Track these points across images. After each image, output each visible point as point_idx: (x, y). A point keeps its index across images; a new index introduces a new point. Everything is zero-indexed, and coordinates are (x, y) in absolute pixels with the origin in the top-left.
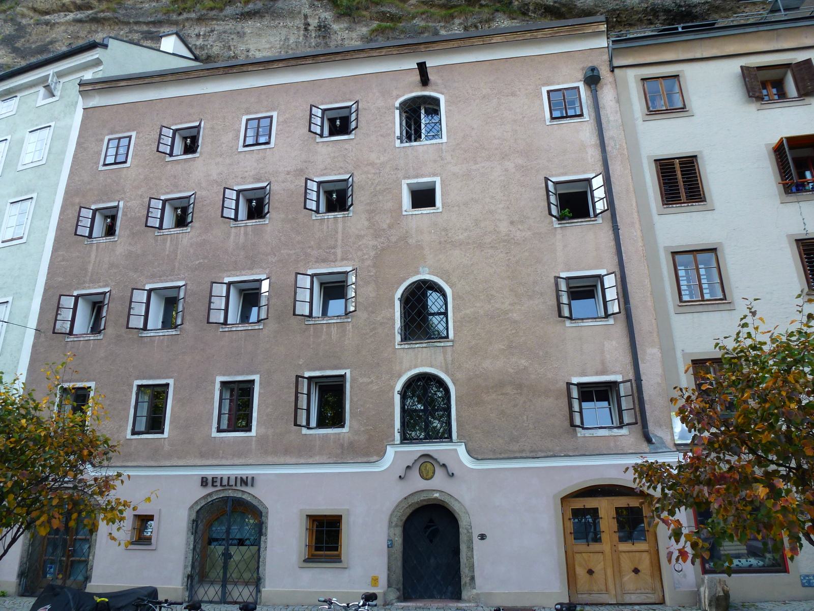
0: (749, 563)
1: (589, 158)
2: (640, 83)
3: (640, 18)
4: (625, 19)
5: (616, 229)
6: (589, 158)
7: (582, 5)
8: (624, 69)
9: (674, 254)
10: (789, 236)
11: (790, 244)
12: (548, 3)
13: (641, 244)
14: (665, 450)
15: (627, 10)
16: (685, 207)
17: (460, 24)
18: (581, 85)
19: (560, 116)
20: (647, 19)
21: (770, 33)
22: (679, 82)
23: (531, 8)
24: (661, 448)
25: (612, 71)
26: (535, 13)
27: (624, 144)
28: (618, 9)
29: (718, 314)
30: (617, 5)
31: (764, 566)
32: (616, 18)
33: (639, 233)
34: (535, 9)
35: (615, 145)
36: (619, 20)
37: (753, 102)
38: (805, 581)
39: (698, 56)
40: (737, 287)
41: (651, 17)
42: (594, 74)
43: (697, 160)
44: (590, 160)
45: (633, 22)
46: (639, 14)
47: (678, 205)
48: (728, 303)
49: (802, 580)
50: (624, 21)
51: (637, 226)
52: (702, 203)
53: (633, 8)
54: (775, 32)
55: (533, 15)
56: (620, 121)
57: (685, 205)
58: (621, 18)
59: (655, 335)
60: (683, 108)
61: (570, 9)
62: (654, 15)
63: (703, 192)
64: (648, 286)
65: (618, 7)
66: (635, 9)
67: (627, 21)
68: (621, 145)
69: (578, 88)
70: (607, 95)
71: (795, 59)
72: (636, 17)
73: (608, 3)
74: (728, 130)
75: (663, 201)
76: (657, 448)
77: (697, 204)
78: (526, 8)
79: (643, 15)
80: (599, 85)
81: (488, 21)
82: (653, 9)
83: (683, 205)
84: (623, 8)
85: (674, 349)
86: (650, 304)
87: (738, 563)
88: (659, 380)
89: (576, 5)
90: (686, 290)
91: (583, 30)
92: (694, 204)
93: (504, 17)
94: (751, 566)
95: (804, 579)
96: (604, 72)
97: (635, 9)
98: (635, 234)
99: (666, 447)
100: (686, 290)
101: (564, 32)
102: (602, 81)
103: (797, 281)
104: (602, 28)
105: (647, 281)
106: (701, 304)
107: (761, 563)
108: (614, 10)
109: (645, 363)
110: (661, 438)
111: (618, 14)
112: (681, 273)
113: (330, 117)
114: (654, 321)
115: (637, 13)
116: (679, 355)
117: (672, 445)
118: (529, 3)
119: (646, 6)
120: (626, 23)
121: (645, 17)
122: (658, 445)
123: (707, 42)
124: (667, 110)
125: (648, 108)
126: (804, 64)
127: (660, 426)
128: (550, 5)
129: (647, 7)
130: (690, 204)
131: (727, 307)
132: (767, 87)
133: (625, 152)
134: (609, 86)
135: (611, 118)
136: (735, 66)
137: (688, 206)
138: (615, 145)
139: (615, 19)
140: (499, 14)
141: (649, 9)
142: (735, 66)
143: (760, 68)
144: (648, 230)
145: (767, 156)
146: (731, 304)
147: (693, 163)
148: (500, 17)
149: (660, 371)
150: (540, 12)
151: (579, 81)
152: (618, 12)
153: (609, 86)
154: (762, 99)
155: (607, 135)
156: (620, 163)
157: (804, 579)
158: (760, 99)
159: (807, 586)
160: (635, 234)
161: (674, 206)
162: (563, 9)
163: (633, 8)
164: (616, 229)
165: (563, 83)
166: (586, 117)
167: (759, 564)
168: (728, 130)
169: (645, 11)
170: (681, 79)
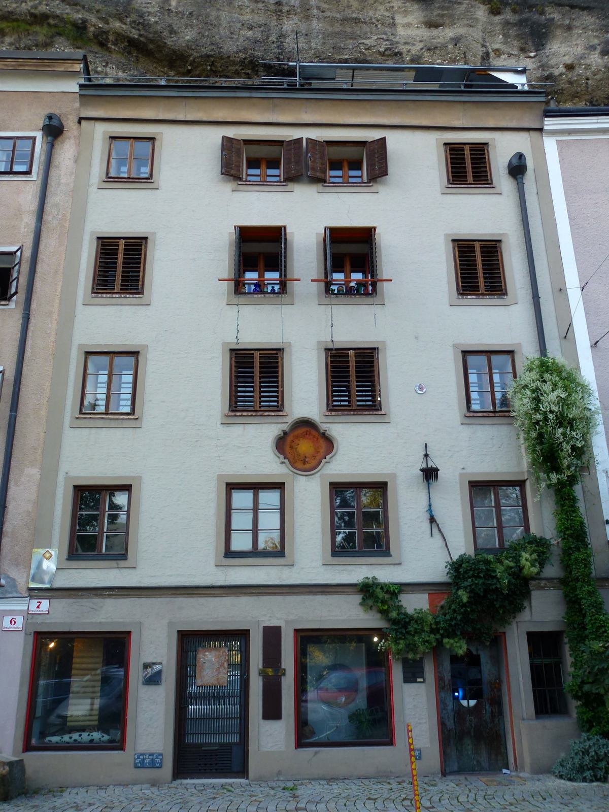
0: (90, 738)
1: (23, 226)
2: (108, 141)
3: (237, 70)
4: (221, 70)
5: (27, 318)
6: (23, 226)
7: (172, 43)
8: (93, 122)
9: (465, 353)
10: (455, 346)
11: (223, 353)
12: (131, 35)
13: (52, 339)
14: (15, 595)
15: (222, 58)
16: (116, 299)
17: (11, 44)
18: (39, 135)
19: (259, 180)
20: (245, 73)
21: (266, 101)
22: (154, 146)
23: (111, 38)
24: (11, 592)
25: (79, 122)
26: (116, 45)
27: (68, 215)
28: (212, 56)
29: (119, 432)
30: (212, 50)
31: (110, 741)
32: (210, 66)
33: (54, 326)
34: (116, 40)
35: (58, 214)
36: (214, 69)
37: (230, 181)
38: (138, 761)
39: (181, 117)
40: (151, 401)
41: (249, 71)
42: (52, 123)
43: (146, 243)
44: (22, 230)
45: (229, 74)
46: (236, 65)
47: (108, 295)
48: (134, 419)
49: (135, 759)
50: (219, 71)
51: (55, 316)
52: (137, 296)
53: (229, 57)
54: (271, 101)
55: (113, 47)
56: (72, 185)
57: (117, 296)
58: (216, 67)
59: (40, 451)
60: (148, 179)
61: (159, 46)
62: (253, 69)
63: (143, 282)
64: (48, 390)
65: (212, 53)
66: (231, 59)
67: (222, 71)
68: (64, 215)
69: (34, 139)
70: (66, 151)
71: (292, 136)
72: (233, 68)
73: (203, 46)
74: (193, 211)
75: (458, 290)
76: (6, 592)
77: (131, 296)
78: (104, 37)
79: (241, 68)
80: (60, 139)
81: (46, 45)
82: (251, 62)
83: (114, 295)
84: (218, 55)
85: (57, 471)
86: (43, 412)
87: (79, 739)
88: (30, 507)
89: (165, 43)
90: (477, 400)
91: (54, 66)
92: (128, 296)
93: (66, 44)
94: (92, 741)
95: (138, 758)
96: (70, 124)
97: (231, 59)
98: (50, 326)
99: (16, 592)
100: (477, 400)
101: (31, 65)
102: (66, 134)
103: (220, 399)
104: (77, 68)
105: (48, 384)
106: (103, 418)
107: (106, 737)
108: (208, 56)
109: (18, 486)
110: (14, 579)
111: (213, 62)
112: (473, 378)
113: (252, 155)
114: (43, 434)
115: (234, 63)
116: (61, 478)
117: (25, 589)
118: (109, 31)
119: (244, 56)
120: (222, 74)
121: (243, 69)
122: (10, 590)
123: (192, 101)
124: (129, 178)
125: (107, 173)
126: (294, 144)
127: (17, 565)
128: (134, 38)
129: (245, 59)
130: (122, 296)
131: (132, 423)
132: (261, 168)
133: (67, 224)
134: (72, 141)
135: (63, 181)
136: (216, 135)
137: (120, 297)
138: (58, 214)
139: (209, 68)
140: (60, 39)
141: (247, 61)
142: (216, 135)
143: (247, 142)
144: (67, 322)
145: (230, 245)
146: (137, 421)
147: (141, 246)
148: (60, 43)
149: (33, 497)
150: (123, 45)
151: (38, 131)
152: (212, 59)
153: (72, 141)
154: (241, 179)
155: (50, 201)
156: (57, 236)
157: (138, 758)
158: (237, 178)
159: (139, 767)
160: (50, 326)
161: (104, 295)
162: (151, 46)
163: (229, 57)
164: (27, 318)
165: (18, 130)
166: (34, 176)
167: (102, 739)
168: (193, 211)
169: (242, 62)
170: (157, 144)
